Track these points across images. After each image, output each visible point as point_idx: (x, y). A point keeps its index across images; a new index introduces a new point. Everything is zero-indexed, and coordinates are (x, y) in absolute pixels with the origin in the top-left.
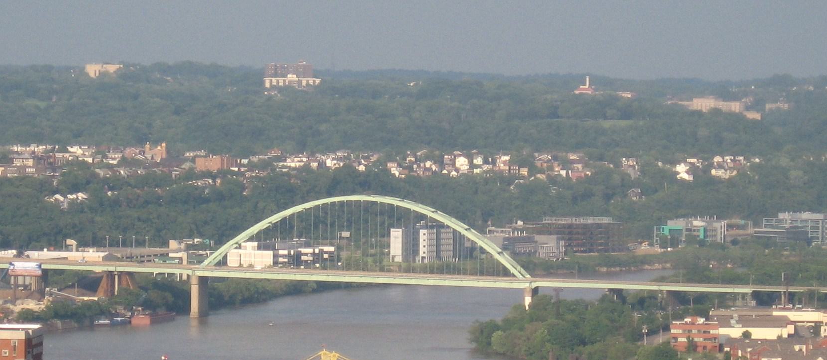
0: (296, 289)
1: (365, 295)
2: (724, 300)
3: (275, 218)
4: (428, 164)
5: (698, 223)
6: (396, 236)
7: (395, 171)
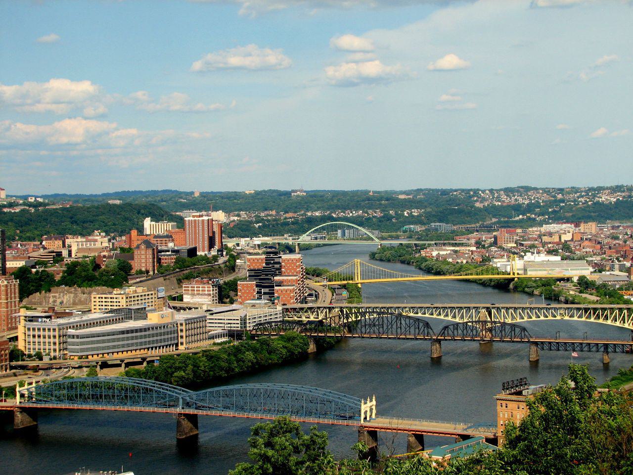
0: (318, 246)
1: (340, 245)
2: (429, 245)
3: (313, 229)
4: (342, 214)
5: (412, 226)
6: (339, 231)
7: (334, 216)
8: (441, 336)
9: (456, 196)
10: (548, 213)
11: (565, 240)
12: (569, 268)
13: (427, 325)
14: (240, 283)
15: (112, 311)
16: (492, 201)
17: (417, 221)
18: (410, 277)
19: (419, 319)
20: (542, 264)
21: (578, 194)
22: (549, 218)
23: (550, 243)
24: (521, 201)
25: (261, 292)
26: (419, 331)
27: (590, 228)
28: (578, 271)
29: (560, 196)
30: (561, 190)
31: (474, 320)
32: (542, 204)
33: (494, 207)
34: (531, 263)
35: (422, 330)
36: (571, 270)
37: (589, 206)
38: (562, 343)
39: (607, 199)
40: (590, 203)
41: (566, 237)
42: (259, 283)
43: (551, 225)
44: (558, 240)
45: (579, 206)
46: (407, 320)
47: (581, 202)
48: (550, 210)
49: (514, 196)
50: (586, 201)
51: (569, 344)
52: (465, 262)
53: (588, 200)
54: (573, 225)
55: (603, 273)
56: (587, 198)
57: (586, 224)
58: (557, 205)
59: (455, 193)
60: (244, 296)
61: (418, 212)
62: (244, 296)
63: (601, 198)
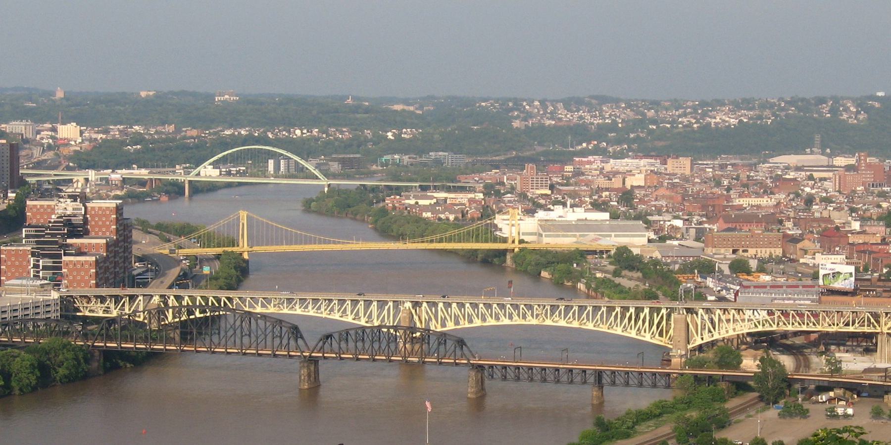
0: (229, 185)
1: (242, 189)
2: (407, 189)
3: (220, 156)
4: (284, 133)
5: (396, 157)
6: (271, 163)
7: (270, 136)
8: (319, 352)
9: (486, 107)
10: (630, 142)
11: (632, 186)
12: (613, 234)
13: (295, 332)
14: (4, 248)
15: (881, 359)
16: (542, 118)
17: (399, 146)
18: (334, 243)
19: (281, 321)
20: (583, 226)
21: (681, 111)
22: (630, 149)
23: (607, 189)
24: (588, 118)
25: (39, 265)
26: (446, 352)
27: (680, 166)
28: (628, 238)
29: (651, 113)
30: (655, 104)
31: (391, 324)
32: (620, 125)
33: (542, 127)
34: (550, 223)
35: (451, 351)
36: (616, 236)
37: (693, 131)
38: (537, 369)
39: (724, 121)
40: (695, 126)
41: (637, 180)
42: (37, 248)
43: (623, 160)
44: (621, 186)
45: (677, 130)
46: (261, 323)
47: (681, 123)
48: (632, 136)
49: (578, 111)
50: (704, 120)
51: (537, 369)
52: (452, 217)
53: (694, 121)
54: (658, 161)
55: (668, 242)
56: (691, 117)
57: (675, 160)
58: (643, 128)
59: (483, 104)
60: (10, 271)
61: (363, 132)
62: (10, 271)
63: (715, 118)
